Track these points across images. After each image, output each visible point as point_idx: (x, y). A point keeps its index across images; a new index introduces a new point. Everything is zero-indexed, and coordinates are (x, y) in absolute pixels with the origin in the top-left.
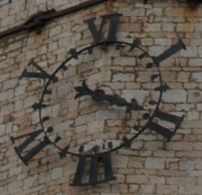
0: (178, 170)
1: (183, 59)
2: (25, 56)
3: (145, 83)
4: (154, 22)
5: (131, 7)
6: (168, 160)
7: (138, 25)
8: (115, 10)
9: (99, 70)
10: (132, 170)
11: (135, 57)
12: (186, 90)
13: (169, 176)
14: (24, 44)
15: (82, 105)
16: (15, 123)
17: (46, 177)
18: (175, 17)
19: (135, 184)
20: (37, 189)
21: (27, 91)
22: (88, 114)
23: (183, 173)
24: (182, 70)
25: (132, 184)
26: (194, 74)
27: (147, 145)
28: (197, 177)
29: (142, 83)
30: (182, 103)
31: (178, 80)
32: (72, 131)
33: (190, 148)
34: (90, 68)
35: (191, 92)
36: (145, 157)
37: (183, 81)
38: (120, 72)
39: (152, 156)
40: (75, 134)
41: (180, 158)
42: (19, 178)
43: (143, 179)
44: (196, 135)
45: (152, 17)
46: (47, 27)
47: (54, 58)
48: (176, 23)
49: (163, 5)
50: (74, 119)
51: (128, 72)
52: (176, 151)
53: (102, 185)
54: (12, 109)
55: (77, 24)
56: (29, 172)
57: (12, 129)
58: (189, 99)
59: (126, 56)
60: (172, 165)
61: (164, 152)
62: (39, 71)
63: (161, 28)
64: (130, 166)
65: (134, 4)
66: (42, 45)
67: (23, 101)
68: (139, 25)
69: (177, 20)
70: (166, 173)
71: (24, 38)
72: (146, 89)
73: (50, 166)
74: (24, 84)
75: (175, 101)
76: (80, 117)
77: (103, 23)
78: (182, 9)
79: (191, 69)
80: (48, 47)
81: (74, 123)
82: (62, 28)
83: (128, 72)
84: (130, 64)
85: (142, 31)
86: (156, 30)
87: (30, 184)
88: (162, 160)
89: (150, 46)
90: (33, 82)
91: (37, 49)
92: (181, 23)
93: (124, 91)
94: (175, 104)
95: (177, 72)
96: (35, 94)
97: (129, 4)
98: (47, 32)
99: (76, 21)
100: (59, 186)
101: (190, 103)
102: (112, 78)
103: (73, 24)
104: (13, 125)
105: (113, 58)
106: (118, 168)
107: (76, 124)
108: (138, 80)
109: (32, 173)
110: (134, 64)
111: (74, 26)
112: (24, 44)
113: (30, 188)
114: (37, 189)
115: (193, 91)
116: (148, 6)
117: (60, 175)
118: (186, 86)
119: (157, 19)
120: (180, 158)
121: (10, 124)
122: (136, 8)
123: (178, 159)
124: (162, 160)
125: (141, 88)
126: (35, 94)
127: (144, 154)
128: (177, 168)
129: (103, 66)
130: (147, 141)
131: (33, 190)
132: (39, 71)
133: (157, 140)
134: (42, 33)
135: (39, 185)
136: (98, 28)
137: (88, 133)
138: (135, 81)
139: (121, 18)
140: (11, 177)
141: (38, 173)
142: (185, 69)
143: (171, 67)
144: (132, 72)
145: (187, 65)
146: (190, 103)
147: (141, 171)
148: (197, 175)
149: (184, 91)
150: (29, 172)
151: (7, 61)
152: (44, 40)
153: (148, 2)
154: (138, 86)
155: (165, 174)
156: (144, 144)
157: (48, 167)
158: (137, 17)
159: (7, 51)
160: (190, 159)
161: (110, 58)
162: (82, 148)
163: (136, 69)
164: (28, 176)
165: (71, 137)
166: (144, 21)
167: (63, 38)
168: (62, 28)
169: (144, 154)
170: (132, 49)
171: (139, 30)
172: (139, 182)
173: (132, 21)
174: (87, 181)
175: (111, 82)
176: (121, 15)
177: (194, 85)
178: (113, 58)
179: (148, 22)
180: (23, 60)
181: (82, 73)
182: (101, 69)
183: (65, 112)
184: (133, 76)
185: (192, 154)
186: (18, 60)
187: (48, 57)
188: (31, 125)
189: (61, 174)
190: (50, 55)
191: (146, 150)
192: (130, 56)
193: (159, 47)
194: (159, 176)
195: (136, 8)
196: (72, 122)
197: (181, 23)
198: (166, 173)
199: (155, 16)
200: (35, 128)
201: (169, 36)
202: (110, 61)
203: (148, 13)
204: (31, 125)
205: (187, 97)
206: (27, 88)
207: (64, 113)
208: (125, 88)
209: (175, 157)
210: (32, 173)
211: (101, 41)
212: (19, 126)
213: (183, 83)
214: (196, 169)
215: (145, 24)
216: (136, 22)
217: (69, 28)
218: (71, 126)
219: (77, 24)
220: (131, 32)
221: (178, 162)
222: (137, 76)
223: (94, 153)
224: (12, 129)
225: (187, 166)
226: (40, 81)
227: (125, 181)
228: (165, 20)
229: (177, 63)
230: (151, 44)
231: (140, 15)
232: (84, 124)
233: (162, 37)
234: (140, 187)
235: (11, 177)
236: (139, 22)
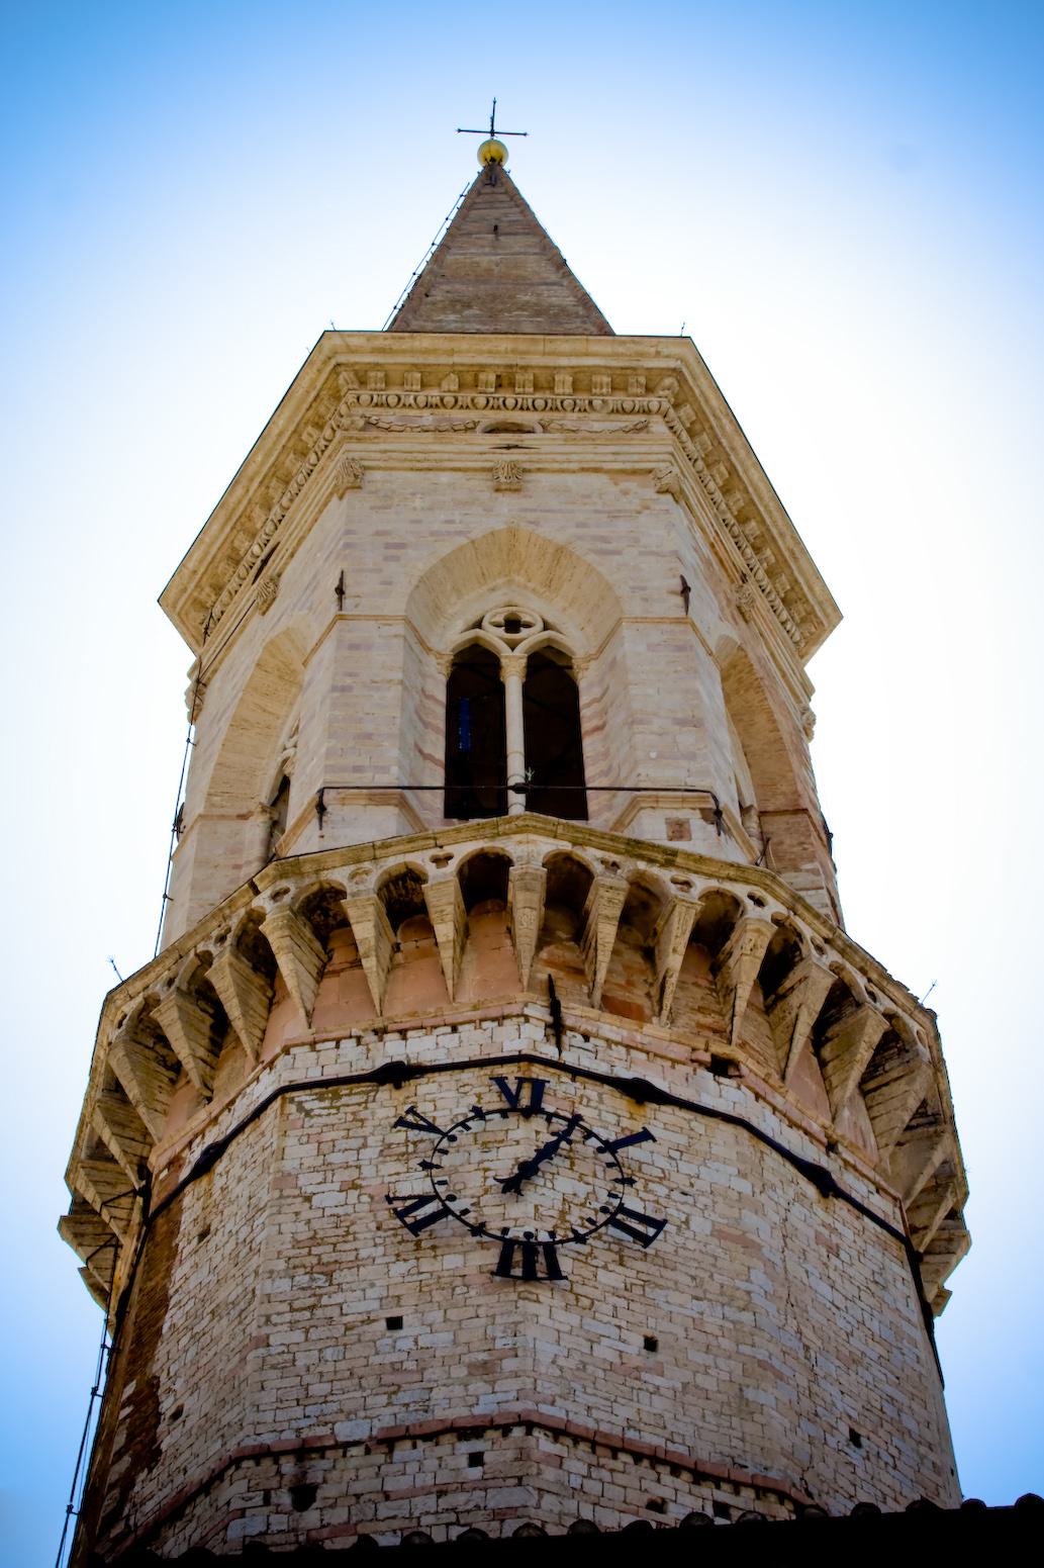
2: (373, 1114)
9: (518, 1142)
33: (658, 1274)
39: (605, 1267)
43: (597, 1294)
52: (638, 1272)
54: (356, 1175)
62: (422, 1123)
70: (627, 1294)
71: (371, 1091)
73: (439, 1252)
105: (537, 1133)
121: (354, 1194)
133: (609, 1250)
141: (417, 1259)
146: (309, 1417)
150: (398, 1255)
151: (340, 1116)
152: (408, 1097)
159: (338, 1104)
169: (595, 1262)
179: (580, 1103)
182: (522, 1142)
185: (661, 1282)
186: (362, 1115)
191: (595, 1258)
198: (627, 1294)
199: (589, 1100)
206: (382, 1151)
209: (637, 1278)
212: (372, 1197)
221: (643, 1286)
227: (276, 1462)
228: (601, 1107)
234: (593, 1303)
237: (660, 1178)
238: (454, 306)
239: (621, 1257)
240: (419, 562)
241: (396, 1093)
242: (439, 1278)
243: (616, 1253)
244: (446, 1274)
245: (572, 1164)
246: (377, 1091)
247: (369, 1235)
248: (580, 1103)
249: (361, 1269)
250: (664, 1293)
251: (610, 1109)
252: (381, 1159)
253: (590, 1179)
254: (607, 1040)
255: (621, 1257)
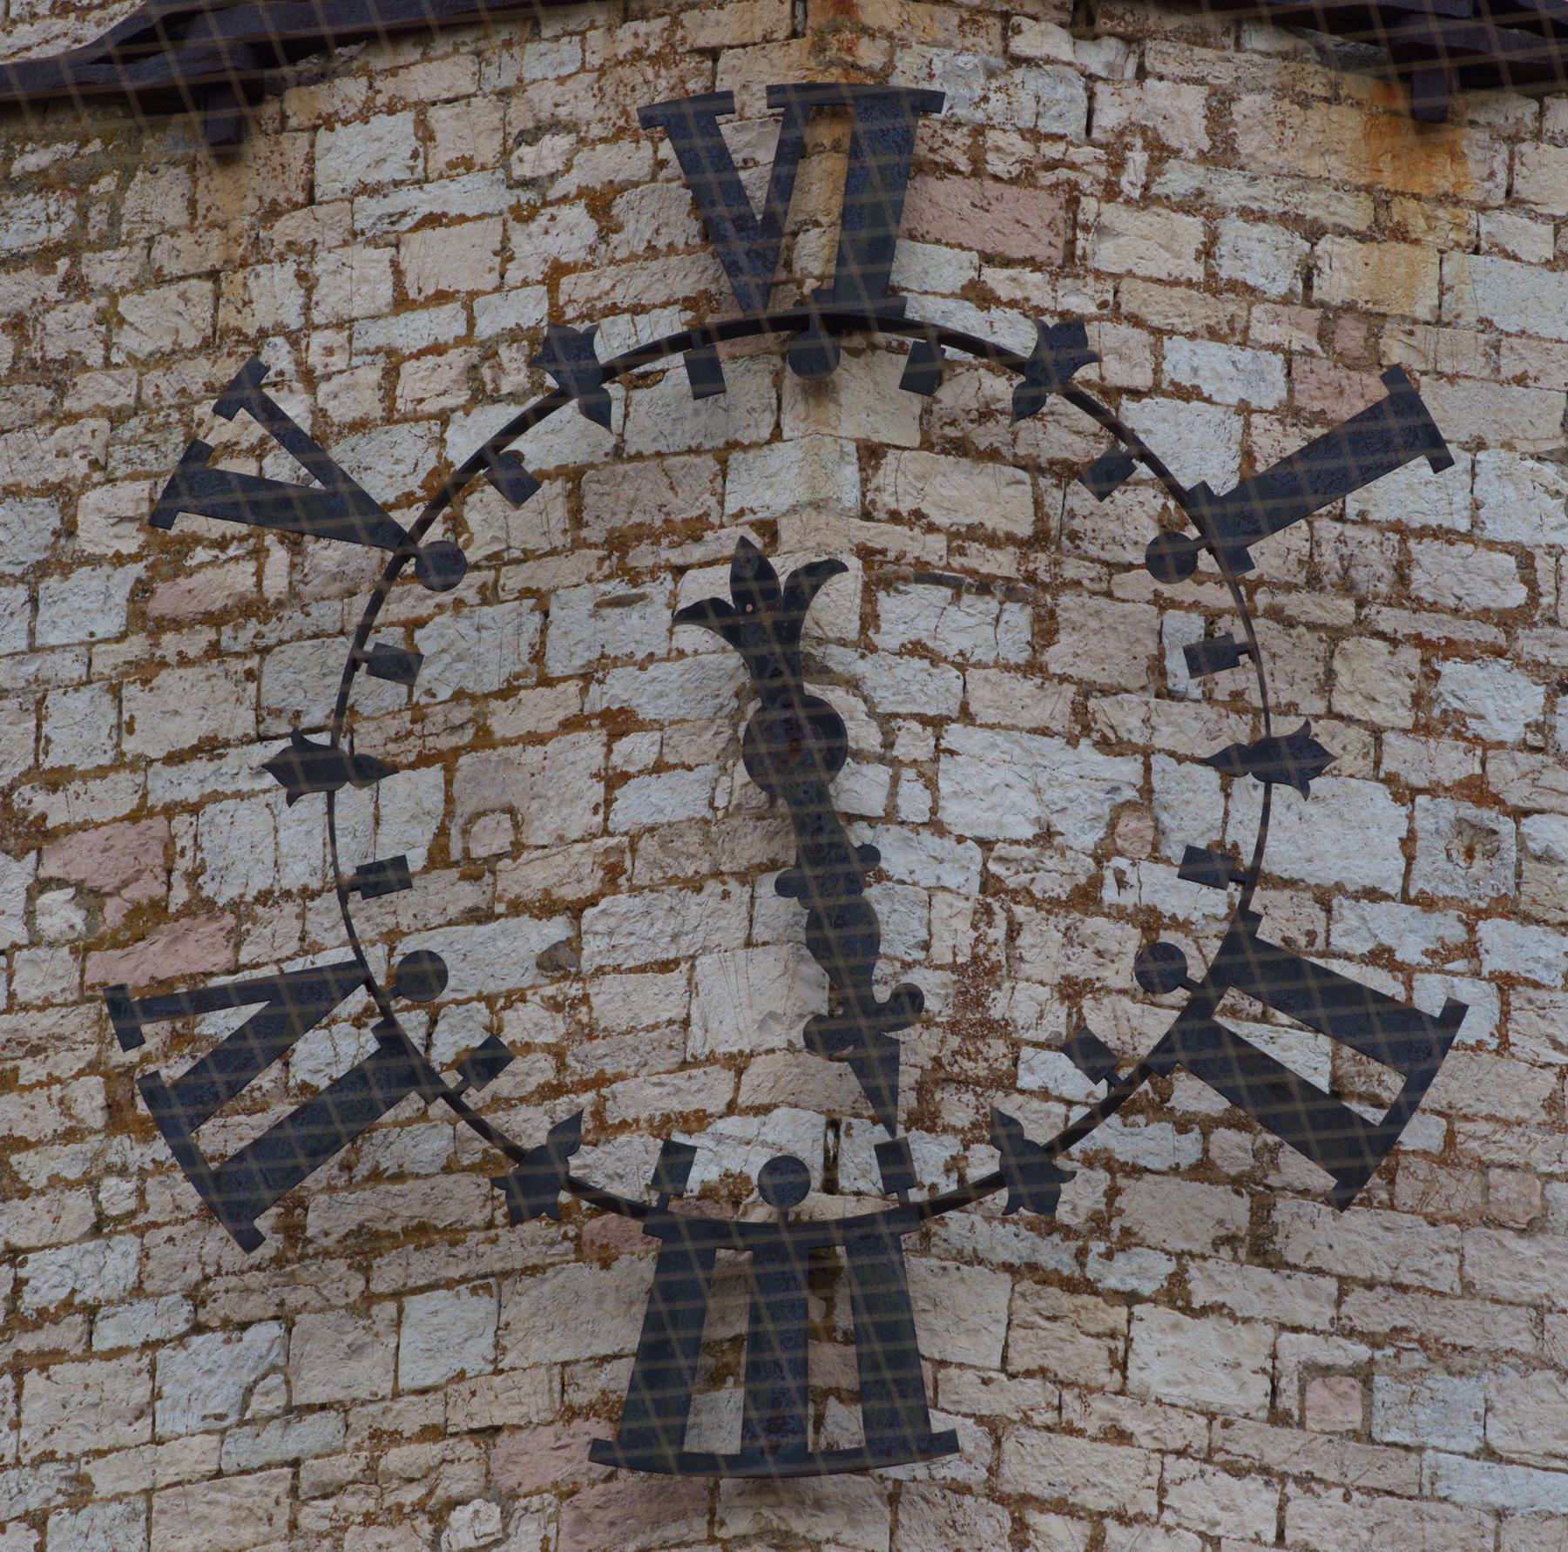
0: (1364, 1436)
1: (1368, 535)
3: (1105, 692)
4: (1147, 199)
5: (987, 41)
6: (1295, 1349)
7: (1041, 207)
8: (870, 54)
10: (1034, 1391)
11: (1032, 467)
12: (1404, 793)
13: (1306, 1481)
14: (98, 219)
15: (633, 807)
16: (51, 869)
17: (355, 1351)
18: (1307, 181)
19: (1063, 1508)
20: (280, 1442)
21: (140, 619)
22: (695, 885)
23: (1400, 1472)
24: (1364, 627)
25: (1042, 1505)
26: (1450, 669)
27: (1137, 1201)
28: (1500, 1514)
29: (1087, 690)
30: (1373, 894)
31: (1343, 704)
32: (555, 1005)
34: (685, 506)
35: (1435, 815)
36: (1131, 1298)
37: (1376, 715)
38: (925, 575)
39: (1175, 1294)
40: (590, 1032)
41: (1374, 1341)
42: (108, 1335)
44: (1484, 1167)
45: (1138, 159)
46: (299, 104)
47: (371, 375)
48: (1314, 232)
49: (1216, 65)
50: (576, 910)
51: (984, 586)
52: (1345, 1284)
53: (830, 1485)
55: (556, 126)
56: (196, 1297)
57: (30, 915)
58: (1422, 865)
59: (960, 448)
60: (1318, 1393)
61: (1261, 1275)
62: (221, 1023)
63: (1207, 252)
64: (1018, 1363)
65: (1009, 30)
66: (256, 254)
67: (115, 691)
68: (1051, 206)
69: (1314, 205)
70: (1279, 1448)
72: (1110, 746)
73: (387, 1274)
74: (119, 560)
75: (1327, 873)
76: (622, 902)
77: (792, 153)
78: (1348, 123)
79: (1434, 629)
80: (304, 279)
81: (574, 944)
82: (426, 135)
83: (984, 586)
84: (995, 522)
85: (1070, 264)
86: (1163, 265)
87: (222, 1398)
88: (1252, 1343)
89: (1136, 394)
90: (201, 554)
91: (213, 275)
92: (1343, 231)
93: (955, 735)
94: (1324, 898)
95: (1335, 635)
96: (214, 651)
97: (973, 19)
98: (294, 148)
99: (544, 99)
100: (467, 1448)
101: (1427, 903)
102: (870, 620)
103: (520, 118)
104: (42, 885)
105: (871, 454)
106: (942, 1364)
107: (593, 951)
108: (1057, 657)
109: (223, 1306)
110: (1025, 529)
111: (531, 136)
112: (98, 219)
113: (217, 1428)
114: (280, 1442)
115: (1448, 809)
116: (1099, 56)
117: (475, 1356)
118: (1401, 754)
119: (1178, 179)
120: (1374, 1341)
122: (1017, 61)
123: (1362, 1352)
124: (1252, 1343)
125: (1082, 724)
126: (214, 651)
127: (1116, 1275)
128: (1355, 1418)
129: (793, 510)
130: (1136, 1171)
131: (241, 1449)
132: (282, 467)
133: (1203, 1170)
134: (259, 146)
135: (295, 1412)
136: (756, 182)
137: (697, 1044)
138: (1033, 668)
139: (926, 127)
140: (43, 1317)
141: (285, 1318)
142: (1389, 619)
143: (1290, 588)
144: (1011, 593)
145: (1402, 592)
146: (1427, 903)
147: (1100, 1405)
148: (1498, 1499)
149: (1380, 795)
152: (272, 212)
153: (1103, 24)
154: (1055, 707)
155: (1273, 1457)
156: (1113, 1193)
157: (366, 1271)
158: (1034, 135)
160: (1443, 1353)
161: (851, 447)
162: (676, 1160)
163: (1040, 562)
164: (198, 1328)
165: (557, 1053)
166: (1085, 183)
167: (432, 220)
168: (426, 135)
169: (1116, 1275)
170: (1027, 407)
171: (1047, 248)
172: (1091, 1499)
173: (996, 165)
174: (728, 1442)
175: (868, 648)
176: (930, 102)
177: (1453, 762)
178: (871, 454)
179: (1111, 191)
180: (95, 356)
181: (618, 543)
183: (491, 838)
184: (1019, 618)
185: (1461, 1324)
187: (315, 358)
188: (201, 906)
189: (485, 1345)
190: (329, 351)
191: (1128, 1240)
192: (993, 455)
193: (1196, 404)
194: (1236, 1471)
195: (1017, 61)
196: (556, 929)
197: (1343, 231)
198: (1279, 1448)
199: (1161, 152)
200: (237, 939)
201: (1266, 330)
202: (851, 473)
203: (1109, 117)
204: (201, 906)
205: (1408, 843)
206: (142, 590)
207: (479, 851)
208: (966, 715)
210: (223, 1306)
211: (784, 304)
212: (90, 897)
213: (1377, 732)
214: (1488, 1453)
215: (1089, 206)
216: (1025, 178)
217: (488, 150)
218: (554, 963)
219: (556, 126)
220: (988, 259)
221: (1364, 1374)
222: (1046, 629)
223: (760, 1213)
224: (30, 915)
225: (1424, 1415)
226: (259, 554)
228: (1230, 189)
229: (1329, 557)
230: (1142, 379)
231: (1046, 126)
232: (666, 966)
233: (1213, 334)
235: (43, 1317)
236: (1047, 178)
237: (1508, 620)
238: (840, 1004)
239: (1262, 1211)
240: (1340, 375)
241: (217, 190)
242: (382, 1438)
243: (1237, 1183)
244: (412, 1416)
245: (1046, 629)
246: (128, 175)
247: (67, 1161)
248: (1111, 191)
249: (33, 1380)
250: (1467, 1392)
251: (1268, 196)
252: (136, 646)
253: (1124, 716)
254: (1442, 293)
255: (1262, 1211)
